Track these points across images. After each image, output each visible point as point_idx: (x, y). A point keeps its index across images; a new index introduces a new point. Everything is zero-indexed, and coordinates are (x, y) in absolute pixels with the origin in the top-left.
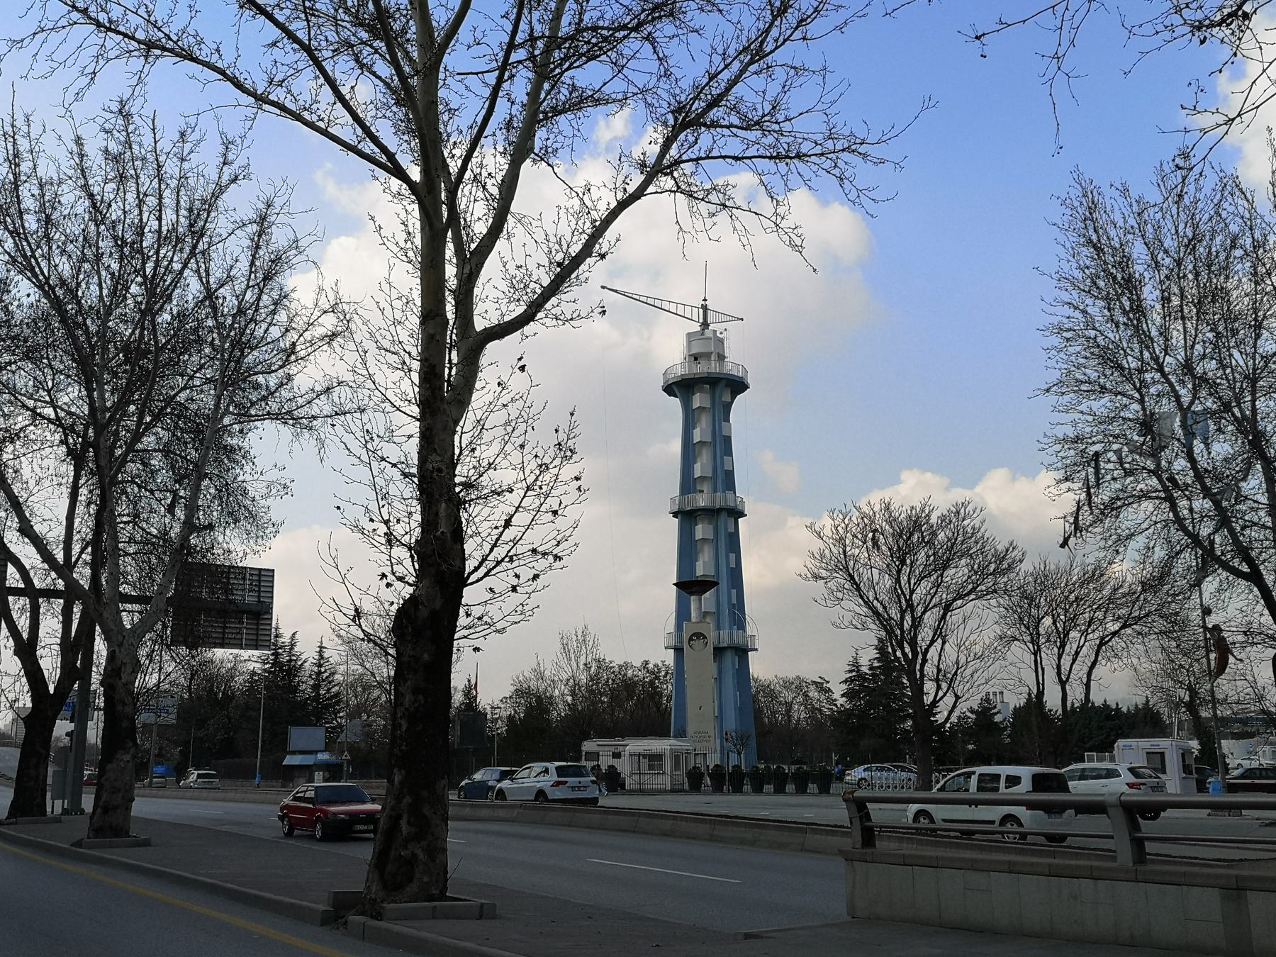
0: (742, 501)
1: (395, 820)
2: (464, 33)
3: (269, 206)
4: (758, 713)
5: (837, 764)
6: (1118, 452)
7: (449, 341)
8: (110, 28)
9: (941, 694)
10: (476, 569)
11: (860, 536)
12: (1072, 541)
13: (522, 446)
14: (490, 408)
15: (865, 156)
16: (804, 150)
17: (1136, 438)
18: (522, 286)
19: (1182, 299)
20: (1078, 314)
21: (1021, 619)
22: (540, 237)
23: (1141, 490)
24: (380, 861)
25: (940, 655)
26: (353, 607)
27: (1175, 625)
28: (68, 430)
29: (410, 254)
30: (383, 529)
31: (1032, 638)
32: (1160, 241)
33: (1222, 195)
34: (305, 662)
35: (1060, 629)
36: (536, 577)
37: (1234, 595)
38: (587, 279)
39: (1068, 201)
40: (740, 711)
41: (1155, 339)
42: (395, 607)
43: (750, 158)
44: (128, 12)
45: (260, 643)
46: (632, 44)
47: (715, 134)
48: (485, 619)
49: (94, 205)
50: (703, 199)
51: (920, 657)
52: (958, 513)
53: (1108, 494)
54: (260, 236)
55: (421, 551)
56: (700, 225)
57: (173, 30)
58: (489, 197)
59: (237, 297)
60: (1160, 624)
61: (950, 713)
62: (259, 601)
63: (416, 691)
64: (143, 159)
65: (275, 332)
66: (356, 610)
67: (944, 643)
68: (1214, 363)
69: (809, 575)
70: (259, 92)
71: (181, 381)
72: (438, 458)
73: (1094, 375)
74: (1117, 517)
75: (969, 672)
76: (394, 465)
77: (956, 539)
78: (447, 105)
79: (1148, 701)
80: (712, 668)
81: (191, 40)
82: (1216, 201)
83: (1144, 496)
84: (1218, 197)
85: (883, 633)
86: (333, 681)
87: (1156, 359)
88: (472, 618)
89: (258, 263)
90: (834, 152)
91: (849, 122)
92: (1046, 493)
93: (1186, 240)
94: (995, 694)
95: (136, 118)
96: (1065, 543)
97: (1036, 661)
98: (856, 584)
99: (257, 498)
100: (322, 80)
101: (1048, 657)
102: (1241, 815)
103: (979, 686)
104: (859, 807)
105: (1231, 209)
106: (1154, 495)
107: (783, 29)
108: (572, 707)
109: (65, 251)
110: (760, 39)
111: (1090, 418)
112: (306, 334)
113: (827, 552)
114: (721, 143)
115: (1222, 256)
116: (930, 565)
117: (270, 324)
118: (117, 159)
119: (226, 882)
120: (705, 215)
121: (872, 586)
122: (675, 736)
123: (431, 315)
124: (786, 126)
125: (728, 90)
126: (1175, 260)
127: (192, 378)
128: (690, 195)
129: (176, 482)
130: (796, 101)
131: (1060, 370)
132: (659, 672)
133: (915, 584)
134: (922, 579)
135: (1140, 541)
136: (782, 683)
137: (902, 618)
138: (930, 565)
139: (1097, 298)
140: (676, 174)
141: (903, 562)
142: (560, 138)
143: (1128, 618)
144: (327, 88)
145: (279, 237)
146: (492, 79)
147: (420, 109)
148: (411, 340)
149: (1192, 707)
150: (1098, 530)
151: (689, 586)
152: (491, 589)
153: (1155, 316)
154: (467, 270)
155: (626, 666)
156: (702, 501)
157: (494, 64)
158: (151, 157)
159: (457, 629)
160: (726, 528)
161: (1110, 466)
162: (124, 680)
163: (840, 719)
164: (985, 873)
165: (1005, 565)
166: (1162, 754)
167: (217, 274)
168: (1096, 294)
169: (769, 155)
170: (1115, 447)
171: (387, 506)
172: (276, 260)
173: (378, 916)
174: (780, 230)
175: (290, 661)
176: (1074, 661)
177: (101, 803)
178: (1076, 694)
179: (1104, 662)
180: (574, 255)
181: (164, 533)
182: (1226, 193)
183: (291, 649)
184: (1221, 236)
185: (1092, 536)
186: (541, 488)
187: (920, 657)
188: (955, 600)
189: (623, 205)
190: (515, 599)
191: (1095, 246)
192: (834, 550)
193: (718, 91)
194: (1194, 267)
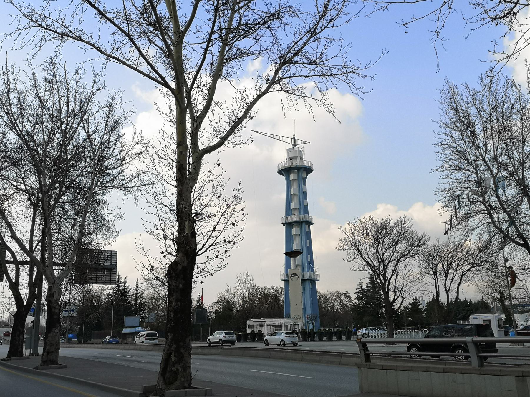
0: (311, 218)
2: (192, 27)
4: (320, 306)
5: (354, 327)
6: (467, 195)
7: (188, 154)
9: (396, 297)
10: (201, 249)
11: (361, 232)
12: (449, 232)
13: (219, 197)
14: (206, 181)
15: (359, 74)
16: (334, 72)
17: (475, 188)
18: (218, 131)
19: (492, 131)
20: (449, 138)
21: (429, 265)
22: (225, 110)
23: (478, 210)
25: (396, 281)
26: (150, 266)
27: (493, 266)
28: (31, 194)
29: (172, 118)
31: (434, 273)
32: (482, 107)
34: (130, 289)
35: (446, 269)
36: (226, 252)
37: (518, 253)
38: (245, 127)
39: (443, 91)
40: (313, 306)
43: (311, 76)
44: (54, 21)
46: (262, 30)
47: (297, 66)
48: (205, 269)
49: (41, 101)
50: (292, 94)
51: (387, 282)
52: (402, 221)
53: (464, 212)
54: (109, 112)
57: (72, 28)
58: (204, 95)
59: (100, 138)
60: (487, 266)
61: (401, 305)
62: (111, 264)
63: (177, 301)
64: (61, 82)
65: (116, 152)
66: (152, 267)
67: (397, 276)
71: (77, 173)
72: (185, 203)
74: (468, 221)
75: (408, 288)
76: (166, 206)
77: (401, 232)
79: (483, 298)
81: (80, 32)
83: (479, 212)
84: (506, 88)
85: (372, 272)
86: (142, 297)
87: (482, 156)
88: (200, 269)
89: (109, 124)
91: (352, 60)
93: (493, 106)
94: (419, 297)
95: (58, 65)
96: (446, 233)
98: (360, 251)
99: (110, 221)
100: (134, 48)
101: (441, 280)
102: (524, 345)
104: (364, 345)
105: (511, 93)
106: (483, 212)
107: (324, 23)
108: (243, 306)
111: (456, 181)
113: (347, 239)
114: (299, 70)
115: (508, 113)
117: (114, 149)
118: (50, 82)
119: (99, 382)
120: (294, 100)
121: (367, 252)
122: (286, 317)
123: (181, 143)
124: (326, 63)
125: (302, 48)
127: (82, 172)
128: (287, 92)
130: (330, 52)
131: (442, 161)
134: (387, 249)
135: (478, 231)
137: (380, 266)
140: (281, 83)
141: (379, 242)
142: (233, 70)
145: (117, 113)
146: (204, 46)
147: (175, 59)
148: (173, 154)
149: (501, 300)
150: (460, 227)
151: (290, 254)
152: (207, 257)
153: (481, 138)
154: (195, 125)
155: (265, 288)
156: (295, 218)
157: (205, 40)
161: (464, 200)
162: (55, 299)
163: (355, 309)
165: (422, 243)
166: (490, 320)
167: (92, 129)
169: (319, 75)
170: (466, 192)
171: (163, 223)
172: (116, 122)
175: (124, 289)
176: (451, 282)
178: (453, 296)
179: (464, 282)
180: (239, 117)
181: (71, 237)
183: (125, 284)
186: (227, 214)
187: (387, 282)
188: (401, 258)
189: (259, 97)
190: (218, 261)
191: (455, 109)
192: (350, 238)
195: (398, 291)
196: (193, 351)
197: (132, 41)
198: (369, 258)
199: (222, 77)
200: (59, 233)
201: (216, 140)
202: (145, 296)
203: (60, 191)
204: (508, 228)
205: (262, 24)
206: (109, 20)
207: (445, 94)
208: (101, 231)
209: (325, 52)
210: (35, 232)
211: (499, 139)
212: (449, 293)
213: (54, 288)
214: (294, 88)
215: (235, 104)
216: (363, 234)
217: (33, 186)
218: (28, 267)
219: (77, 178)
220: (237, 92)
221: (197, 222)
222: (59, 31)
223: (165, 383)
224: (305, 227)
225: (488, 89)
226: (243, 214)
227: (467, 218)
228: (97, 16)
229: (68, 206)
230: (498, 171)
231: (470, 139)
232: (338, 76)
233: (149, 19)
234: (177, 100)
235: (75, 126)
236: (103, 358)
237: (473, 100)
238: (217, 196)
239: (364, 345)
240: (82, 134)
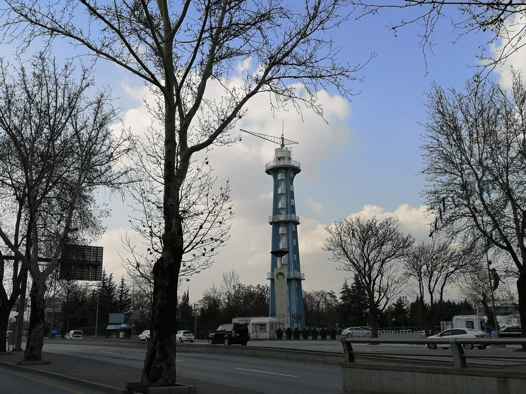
0: (298, 218)
2: (183, 25)
3: (102, 96)
4: (306, 306)
5: (338, 327)
6: (453, 197)
7: (177, 152)
9: (381, 297)
10: (188, 246)
11: (347, 232)
12: (434, 234)
13: (207, 195)
14: (194, 179)
15: (348, 76)
16: (323, 74)
18: (207, 129)
19: (478, 135)
20: (435, 141)
21: (414, 266)
22: (214, 109)
23: (462, 213)
26: (136, 263)
27: (477, 268)
28: (17, 189)
29: (161, 116)
30: (149, 230)
31: (418, 274)
32: (468, 111)
34: (116, 286)
36: (212, 250)
38: (234, 126)
42: (154, 263)
43: (301, 77)
44: (44, 16)
45: (97, 278)
46: (253, 31)
47: (286, 67)
48: (191, 267)
49: (29, 96)
50: (281, 94)
51: (372, 282)
52: (387, 222)
53: (449, 214)
54: (98, 108)
57: (63, 23)
58: (193, 93)
59: (88, 134)
60: (471, 268)
62: (97, 260)
64: (50, 77)
65: (104, 148)
66: (137, 264)
67: (382, 276)
69: (326, 248)
70: (98, 49)
71: (64, 169)
72: (172, 200)
73: (442, 166)
74: (452, 224)
75: (392, 288)
76: (154, 203)
77: (386, 233)
79: (466, 300)
80: (286, 287)
81: (70, 28)
82: (490, 95)
83: (464, 215)
84: (492, 93)
86: (126, 295)
87: (467, 159)
88: (186, 267)
91: (341, 62)
93: (479, 111)
94: (403, 297)
95: (47, 60)
96: (431, 235)
97: (420, 284)
98: (346, 252)
99: (96, 217)
100: (124, 45)
101: (425, 282)
105: (497, 98)
106: (467, 215)
107: (314, 25)
108: (228, 304)
111: (441, 184)
112: (117, 149)
113: (334, 239)
115: (494, 117)
117: (102, 145)
118: (39, 77)
119: (82, 379)
122: (271, 316)
123: (169, 141)
124: (316, 64)
125: (292, 49)
127: (69, 167)
128: (276, 92)
131: (428, 164)
132: (264, 289)
134: (373, 250)
135: (462, 234)
137: (365, 266)
139: (443, 134)
140: (270, 84)
141: (365, 243)
142: (223, 69)
144: (126, 48)
145: (106, 109)
146: (195, 44)
148: (161, 151)
149: (484, 302)
150: (445, 229)
151: (276, 253)
152: (194, 255)
153: (467, 142)
154: (184, 123)
155: (250, 287)
156: (282, 218)
157: (196, 39)
158: (53, 76)
161: (449, 203)
162: (39, 294)
165: (407, 244)
166: (472, 322)
167: (80, 124)
170: (451, 195)
172: (105, 119)
175: (110, 285)
176: (436, 283)
178: (436, 297)
179: (448, 284)
180: (228, 116)
181: (57, 232)
182: (495, 92)
183: (110, 280)
186: (215, 212)
187: (372, 282)
188: (386, 258)
189: (249, 96)
190: (204, 259)
191: (441, 113)
194: (482, 122)
196: (177, 348)
197: (122, 38)
198: (354, 258)
199: (211, 76)
201: (205, 138)
206: (99, 16)
208: (88, 227)
210: (20, 227)
212: (433, 294)
215: (224, 103)
221: (184, 220)
225: (475, 94)
226: (231, 212)
227: (452, 220)
230: (483, 175)
232: (327, 78)
236: (87, 354)
237: (460, 105)
238: (204, 195)
239: (348, 345)
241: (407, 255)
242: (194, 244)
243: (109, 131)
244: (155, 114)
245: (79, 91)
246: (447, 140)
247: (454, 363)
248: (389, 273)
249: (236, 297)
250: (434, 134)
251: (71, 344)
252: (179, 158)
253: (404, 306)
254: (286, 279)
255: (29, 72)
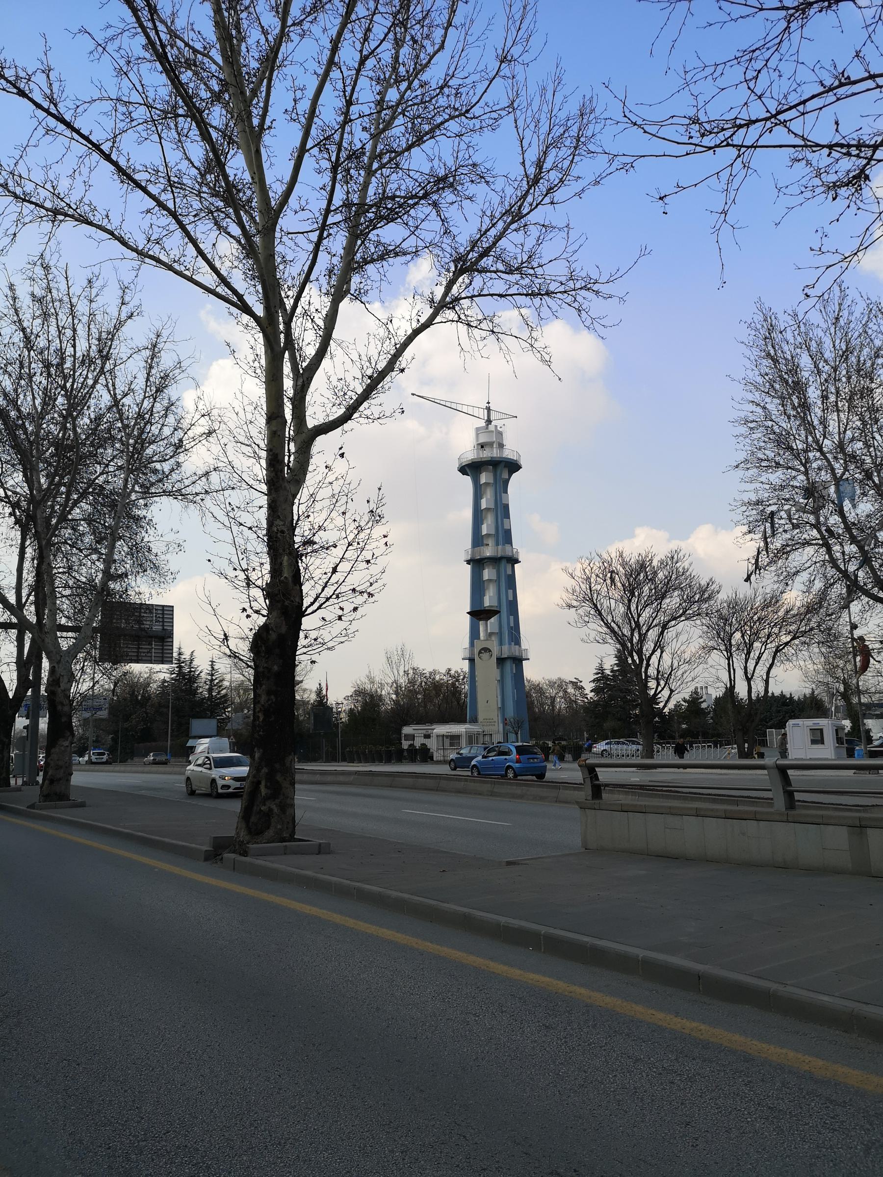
0: (517, 552)
1: (256, 785)
2: (293, 201)
3: (158, 336)
4: (530, 705)
5: (588, 740)
6: (788, 512)
7: (287, 436)
8: (24, 199)
9: (660, 689)
10: (312, 604)
11: (601, 576)
12: (753, 578)
13: (344, 513)
14: (320, 485)
15: (597, 293)
16: (552, 288)
17: (801, 500)
18: (342, 393)
19: (837, 397)
20: (759, 410)
21: (719, 634)
22: (355, 357)
23: (805, 539)
24: (246, 814)
25: (659, 661)
26: (222, 633)
27: (830, 637)
28: (15, 505)
29: (258, 371)
30: (242, 576)
31: (726, 648)
32: (821, 353)
33: (869, 317)
34: (201, 672)
35: (747, 641)
36: (355, 609)
37: (874, 614)
38: (389, 388)
39: (753, 325)
40: (517, 703)
41: (817, 427)
42: (254, 631)
43: (511, 295)
44: (38, 187)
45: (165, 659)
46: (423, 210)
47: (485, 277)
48: (319, 640)
49: (25, 337)
50: (476, 327)
51: (645, 662)
52: (673, 557)
53: (781, 542)
54: (152, 359)
55: (270, 592)
56: (475, 347)
57: (73, 199)
58: (316, 328)
59: (138, 405)
60: (819, 637)
61: (667, 702)
62: (163, 629)
63: (269, 693)
64: (61, 301)
65: (167, 431)
66: (225, 635)
67: (662, 652)
68: (860, 445)
69: (564, 605)
70: (140, 248)
71: (99, 469)
72: (282, 523)
73: (771, 455)
74: (787, 559)
75: (680, 672)
76: (250, 528)
77: (671, 577)
78: (284, 257)
79: (813, 692)
80: (495, 673)
81: (87, 208)
82: (863, 322)
83: (807, 543)
84: (866, 319)
85: (618, 646)
86: (221, 686)
87: (816, 441)
88: (309, 640)
89: (151, 379)
90: (574, 290)
91: (585, 267)
92: (735, 542)
93: (841, 352)
94: (702, 688)
95: (53, 269)
96: (748, 579)
97: (729, 664)
98: (598, 610)
99: (159, 554)
100: (186, 240)
101: (738, 662)
102: (878, 773)
103: (687, 682)
104: (591, 770)
105: (875, 328)
106: (814, 542)
107: (536, 196)
108: (396, 702)
109: (6, 371)
110: (519, 204)
111: (767, 487)
112: (189, 433)
113: (578, 588)
114: (489, 284)
115: (869, 363)
116: (652, 596)
117: (163, 425)
118: (40, 301)
119: (139, 831)
120: (478, 338)
121: (610, 612)
122: (470, 722)
123: (274, 416)
124: (539, 271)
125: (494, 244)
126: (832, 367)
127: (107, 465)
128: (469, 325)
129: (97, 542)
130: (548, 251)
131: (746, 451)
132: (459, 676)
133: (641, 610)
134: (647, 606)
135: (804, 576)
136: (547, 682)
137: (632, 635)
138: (652, 596)
139: (774, 397)
140: (457, 308)
141: (633, 595)
142: (369, 282)
143: (797, 632)
144: (190, 245)
145: (166, 360)
146: (314, 236)
147: (262, 261)
148: (260, 435)
149: (845, 696)
150: (773, 568)
151: (478, 614)
152: (323, 618)
153: (817, 410)
154: (300, 383)
155: (434, 672)
156: (488, 552)
157: (316, 226)
158: (66, 299)
159: (298, 648)
160: (506, 571)
161: (782, 522)
162: (62, 688)
163: (591, 708)
164: (680, 817)
165: (706, 595)
166: (821, 730)
167: (121, 388)
168: (773, 394)
169: (525, 292)
170: (786, 507)
171: (245, 559)
172: (165, 377)
173: (245, 853)
174: (534, 349)
175: (191, 671)
176: (757, 663)
177: (48, 777)
178: (758, 687)
179: (778, 664)
180: (380, 370)
181: (91, 580)
182: (872, 316)
183: (191, 663)
184: (867, 349)
185: (768, 573)
186: (358, 544)
187: (645, 662)
188: (669, 621)
189: (416, 332)
190: (340, 625)
191: (772, 359)
192: (583, 586)
193: (487, 245)
194: (847, 372)
195: (665, 678)
196: (298, 777)
197: (182, 227)
198: (614, 622)
199: (349, 295)
200: (69, 574)
201: (338, 411)
202: (226, 683)
203: (68, 499)
204: (858, 569)
205: (421, 198)
206: (138, 185)
207: (756, 330)
208: (145, 571)
209: (538, 251)
210: (25, 572)
211: (849, 413)
212: (752, 683)
213: (60, 670)
214: (480, 317)
215: (372, 345)
216: (605, 581)
217: (18, 490)
218: (14, 633)
219: (99, 476)
220: (377, 324)
221: (303, 558)
222: (48, 205)
223: (250, 831)
224: (506, 567)
225: (834, 321)
226: (386, 543)
227: (787, 553)
228: (116, 177)
229: (83, 527)
230: (846, 469)
231: (797, 412)
232: (559, 295)
233: (215, 185)
234: (266, 336)
235: (90, 382)
236: (155, 789)
237: (805, 341)
238: (340, 512)
239: (591, 770)
240: (102, 398)
241: (707, 614)
242: (322, 600)
243: (173, 399)
244: (246, 368)
245: (115, 326)
246: (780, 406)
247: (772, 799)
248: (673, 646)
249: (410, 691)
250: (757, 396)
251: (124, 772)
252: (292, 447)
253: (702, 702)
254: (494, 660)
255: (23, 291)
